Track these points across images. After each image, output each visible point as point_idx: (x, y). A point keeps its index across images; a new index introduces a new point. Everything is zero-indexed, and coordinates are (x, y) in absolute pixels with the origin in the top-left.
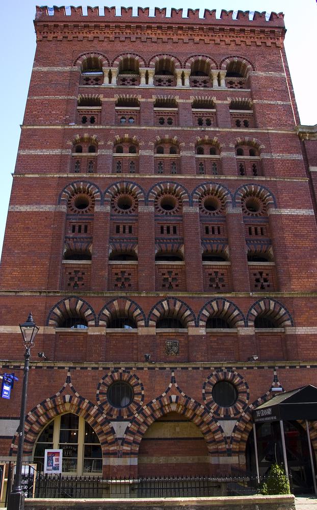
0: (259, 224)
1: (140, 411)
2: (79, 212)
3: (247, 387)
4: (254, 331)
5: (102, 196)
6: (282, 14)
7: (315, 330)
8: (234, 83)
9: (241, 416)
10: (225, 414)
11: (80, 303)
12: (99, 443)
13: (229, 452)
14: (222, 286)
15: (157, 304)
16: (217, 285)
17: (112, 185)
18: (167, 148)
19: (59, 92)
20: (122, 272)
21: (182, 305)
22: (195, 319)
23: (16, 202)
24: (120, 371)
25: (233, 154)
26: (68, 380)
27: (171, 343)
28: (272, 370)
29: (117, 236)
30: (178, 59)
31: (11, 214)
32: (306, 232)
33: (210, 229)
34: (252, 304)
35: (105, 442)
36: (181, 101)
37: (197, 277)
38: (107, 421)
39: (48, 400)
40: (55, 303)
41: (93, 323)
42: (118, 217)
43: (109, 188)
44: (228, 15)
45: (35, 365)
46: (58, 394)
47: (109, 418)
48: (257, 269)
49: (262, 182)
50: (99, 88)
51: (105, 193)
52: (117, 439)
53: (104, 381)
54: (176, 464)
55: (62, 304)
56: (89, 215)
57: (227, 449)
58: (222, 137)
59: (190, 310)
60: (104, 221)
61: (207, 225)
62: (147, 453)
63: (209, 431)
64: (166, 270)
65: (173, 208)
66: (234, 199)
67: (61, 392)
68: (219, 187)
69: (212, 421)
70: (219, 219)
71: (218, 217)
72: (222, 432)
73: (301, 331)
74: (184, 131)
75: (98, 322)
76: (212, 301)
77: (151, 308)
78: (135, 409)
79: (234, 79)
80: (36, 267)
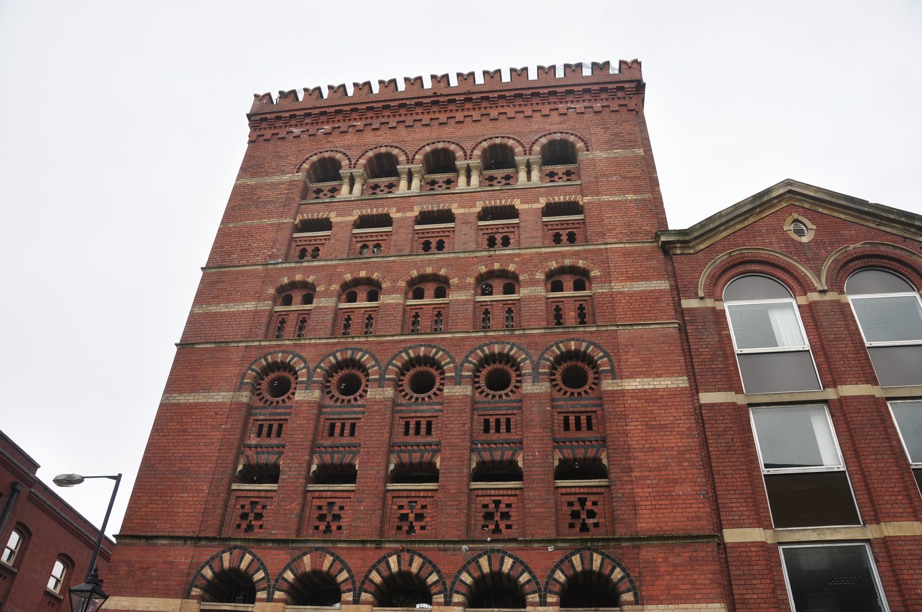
0: (583, 409)
2: (272, 403)
5: (310, 375)
6: (637, 63)
8: (557, 174)
11: (248, 558)
14: (506, 528)
15: (379, 562)
16: (497, 526)
17: (329, 355)
18: (430, 288)
19: (269, 214)
20: (579, 499)
21: (424, 563)
22: (445, 589)
23: (175, 389)
25: (540, 291)
29: (328, 442)
30: (461, 147)
31: (165, 411)
32: (672, 418)
36: (461, 211)
40: (206, 558)
41: (440, 598)
42: (334, 410)
43: (322, 361)
44: (546, 73)
48: (491, 496)
49: (590, 335)
50: (331, 202)
51: (315, 370)
55: (217, 560)
56: (359, 406)
58: (525, 264)
59: (438, 572)
60: (306, 415)
61: (487, 417)
64: (406, 499)
65: (585, 383)
66: (535, 367)
68: (511, 349)
70: (510, 405)
74: (460, 258)
76: (480, 556)
77: (367, 569)
79: (559, 169)
80: (186, 495)
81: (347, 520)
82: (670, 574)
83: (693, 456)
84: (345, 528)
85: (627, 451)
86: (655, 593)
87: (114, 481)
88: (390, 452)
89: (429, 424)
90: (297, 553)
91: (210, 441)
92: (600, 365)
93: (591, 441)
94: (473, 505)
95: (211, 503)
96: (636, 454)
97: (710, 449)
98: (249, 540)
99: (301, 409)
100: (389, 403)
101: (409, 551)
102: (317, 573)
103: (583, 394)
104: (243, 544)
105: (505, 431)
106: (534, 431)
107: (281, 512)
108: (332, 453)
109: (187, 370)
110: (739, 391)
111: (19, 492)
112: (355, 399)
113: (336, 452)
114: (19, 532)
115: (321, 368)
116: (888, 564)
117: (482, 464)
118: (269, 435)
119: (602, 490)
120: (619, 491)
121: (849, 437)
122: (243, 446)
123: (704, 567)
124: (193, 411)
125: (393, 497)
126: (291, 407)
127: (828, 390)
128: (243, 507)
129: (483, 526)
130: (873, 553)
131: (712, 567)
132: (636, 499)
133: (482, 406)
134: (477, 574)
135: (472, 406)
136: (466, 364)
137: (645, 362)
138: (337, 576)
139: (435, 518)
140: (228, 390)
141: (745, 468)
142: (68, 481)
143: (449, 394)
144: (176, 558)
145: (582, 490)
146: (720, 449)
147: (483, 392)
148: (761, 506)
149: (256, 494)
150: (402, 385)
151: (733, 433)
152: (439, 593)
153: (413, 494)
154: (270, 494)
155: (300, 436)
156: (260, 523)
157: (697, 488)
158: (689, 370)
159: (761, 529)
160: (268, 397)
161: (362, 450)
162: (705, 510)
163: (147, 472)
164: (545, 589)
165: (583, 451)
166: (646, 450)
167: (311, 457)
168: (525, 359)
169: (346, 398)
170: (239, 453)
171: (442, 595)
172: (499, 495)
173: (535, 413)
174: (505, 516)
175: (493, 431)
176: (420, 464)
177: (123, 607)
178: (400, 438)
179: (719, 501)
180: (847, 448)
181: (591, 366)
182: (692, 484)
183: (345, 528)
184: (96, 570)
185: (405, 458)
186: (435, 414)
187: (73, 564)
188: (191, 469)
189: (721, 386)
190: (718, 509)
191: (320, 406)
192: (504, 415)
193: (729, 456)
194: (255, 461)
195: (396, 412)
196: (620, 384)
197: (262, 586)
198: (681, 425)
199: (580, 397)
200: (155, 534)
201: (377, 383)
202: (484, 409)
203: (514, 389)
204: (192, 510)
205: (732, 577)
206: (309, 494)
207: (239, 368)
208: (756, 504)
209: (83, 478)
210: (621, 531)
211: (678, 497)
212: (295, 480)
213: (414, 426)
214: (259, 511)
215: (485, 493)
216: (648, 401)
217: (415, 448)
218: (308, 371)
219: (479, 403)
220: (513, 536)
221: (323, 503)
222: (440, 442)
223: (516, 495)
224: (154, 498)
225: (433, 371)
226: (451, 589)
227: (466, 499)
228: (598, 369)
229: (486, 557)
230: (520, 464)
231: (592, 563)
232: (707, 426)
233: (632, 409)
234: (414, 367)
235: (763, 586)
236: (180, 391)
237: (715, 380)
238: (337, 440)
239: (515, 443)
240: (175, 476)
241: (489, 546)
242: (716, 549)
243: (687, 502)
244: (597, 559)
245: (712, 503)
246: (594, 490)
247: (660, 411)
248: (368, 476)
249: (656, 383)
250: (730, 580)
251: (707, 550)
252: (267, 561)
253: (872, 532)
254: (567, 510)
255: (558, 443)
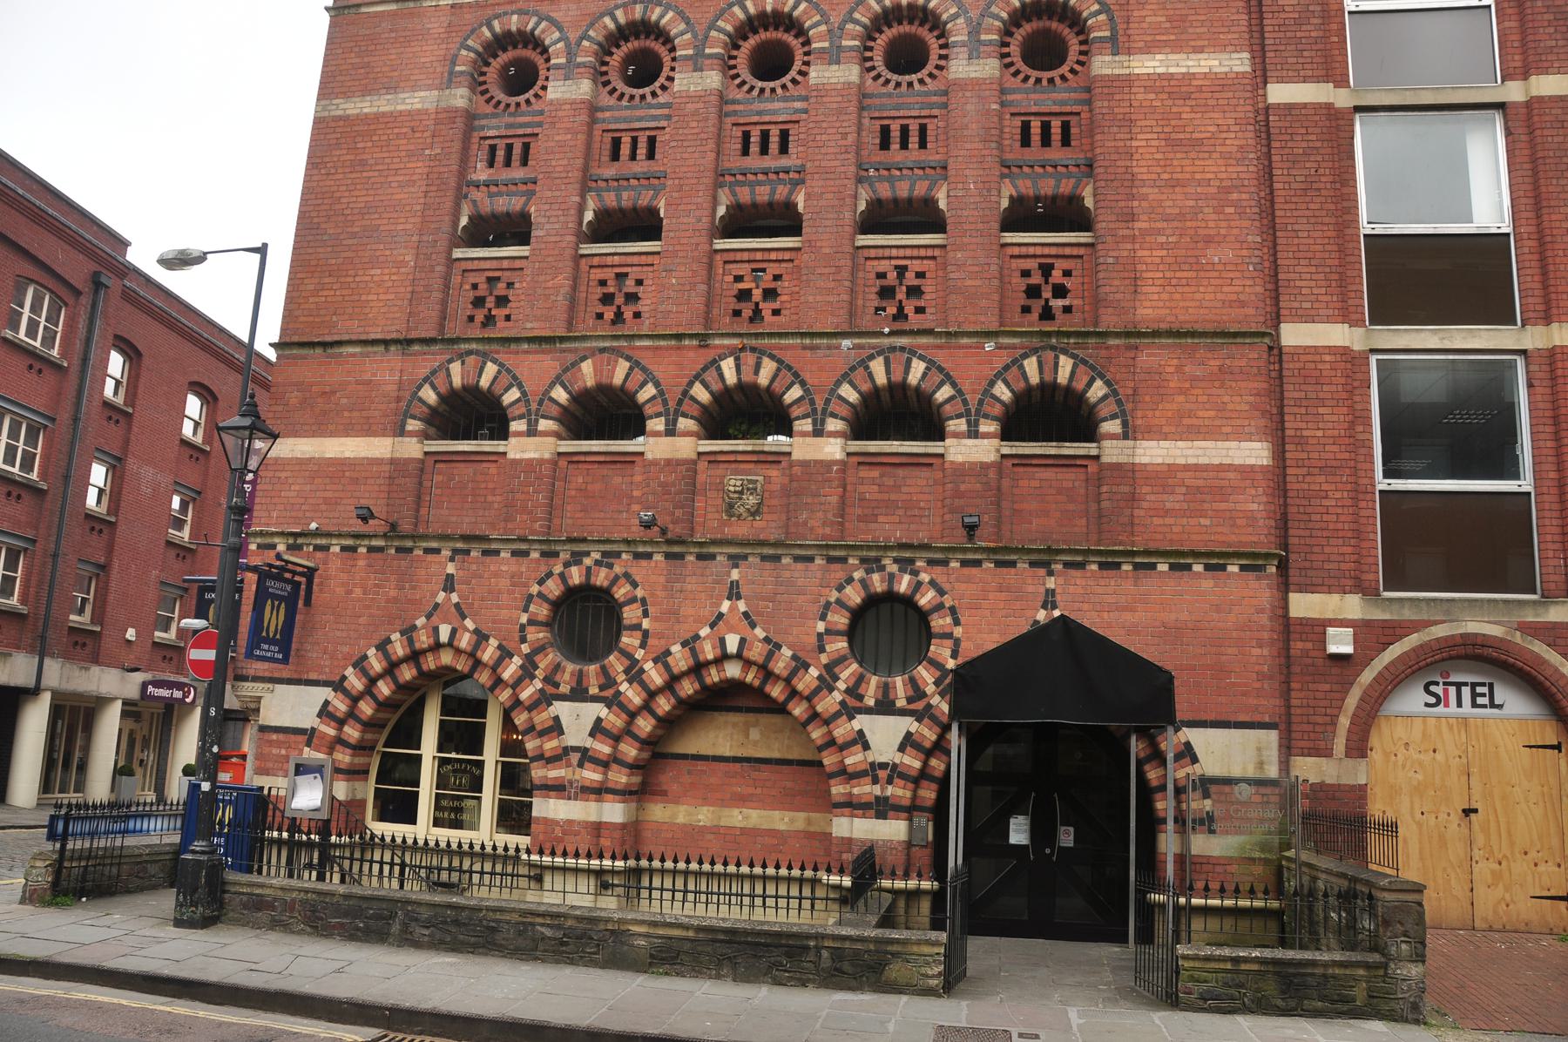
0: (1056, 109)
1: (635, 674)
2: (508, 105)
3: (957, 622)
4: (998, 451)
5: (570, 54)
7: (1200, 452)
9: (929, 706)
10: (880, 697)
11: (491, 369)
12: (526, 756)
13: (882, 808)
15: (705, 369)
16: (901, 308)
17: (602, 15)
20: (1041, 266)
21: (778, 370)
22: (814, 411)
23: (336, 90)
24: (587, 561)
26: (449, 584)
27: (739, 483)
28: (1042, 572)
29: (610, 171)
31: (322, 127)
33: (895, 134)
34: (1000, 366)
35: (540, 757)
37: (832, 285)
38: (544, 699)
39: (395, 636)
40: (425, 372)
42: (616, 114)
43: (592, 25)
45: (366, 542)
46: (421, 622)
47: (550, 690)
48: (890, 258)
52: (567, 750)
53: (542, 589)
54: (744, 831)
56: (661, 106)
57: (877, 798)
59: (803, 384)
61: (886, 122)
62: (664, 793)
63: (831, 742)
64: (746, 265)
66: (975, 31)
67: (428, 617)
69: (837, 715)
70: (926, 99)
71: (927, 94)
72: (866, 747)
73: (1152, 452)
75: (537, 421)
76: (872, 357)
77: (686, 380)
78: (620, 669)
80: (379, 271)
81: (649, 302)
82: (1182, 391)
83: (1244, 196)
84: (647, 315)
85: (1129, 184)
86: (1156, 421)
87: (257, 257)
88: (717, 185)
89: (784, 135)
90: (570, 358)
91: (407, 178)
92: (1092, 29)
93: (1067, 166)
94: (861, 274)
95: (422, 282)
96: (1144, 190)
97: (1276, 186)
98: (490, 340)
99: (560, 114)
100: (712, 98)
101: (753, 349)
102: (604, 389)
103: (1058, 81)
104: (480, 347)
105: (917, 146)
106: (968, 146)
107: (539, 291)
108: (618, 190)
109: (353, 55)
110: (1342, 82)
111: (107, 287)
112: (654, 94)
113: (625, 189)
114: (122, 351)
115: (589, 39)
116: (1548, 391)
117: (876, 204)
118: (508, 163)
119: (1082, 251)
120: (1111, 254)
121: (1530, 173)
122: (464, 185)
123: (1243, 384)
124: (372, 127)
125: (725, 262)
126: (541, 113)
127: (1510, 84)
128: (475, 287)
129: (877, 309)
130: (1527, 372)
131: (1256, 385)
132: (1139, 267)
133: (877, 101)
134: (866, 387)
135: (860, 102)
136: (849, 26)
137: (1175, 24)
138: (637, 392)
139: (796, 296)
140: (429, 88)
141: (1333, 220)
142: (180, 260)
143: (819, 81)
144: (374, 375)
145: (1046, 251)
146: (1294, 186)
147: (879, 76)
148: (1351, 288)
149: (494, 264)
150: (734, 67)
151: (1319, 158)
152: (805, 416)
153: (759, 256)
154: (518, 264)
155: (561, 162)
156: (506, 311)
157: (1245, 252)
158: (1254, 41)
159: (1346, 325)
160: (500, 96)
161: (669, 182)
162: (1254, 290)
163: (310, 238)
164: (978, 413)
165: (1052, 182)
166: (1163, 183)
167: (583, 197)
168: (955, 17)
169: (638, 92)
170: (460, 197)
171: (810, 420)
172: (905, 258)
173: (971, 114)
174: (915, 292)
175: (895, 146)
176: (770, 204)
177: (303, 452)
178: (734, 161)
179: (1280, 276)
180: (1522, 193)
181: (1075, 30)
182: (1238, 245)
183: (647, 315)
184: (252, 396)
185: (745, 195)
186: (794, 118)
187: (215, 399)
188: (382, 228)
189: (1310, 73)
190: (1276, 290)
191: (593, 109)
192: (915, 117)
193: (1307, 199)
194: (488, 209)
195: (727, 115)
196: (1126, 64)
197: (517, 413)
198: (1228, 142)
199: (1051, 87)
200: (336, 338)
201: (690, 63)
202: (881, 108)
203: (935, 72)
204: (392, 297)
205: (1286, 402)
206: (583, 261)
207: (444, 46)
208: (1343, 284)
209: (205, 254)
210: (1109, 321)
211: (1209, 267)
212: (558, 238)
213: (758, 139)
214: (503, 293)
215: (881, 253)
216: (1174, 96)
217: (761, 177)
218: (568, 45)
219: (871, 96)
220: (927, 326)
221: (609, 274)
222: (803, 165)
223: (934, 258)
224: (326, 280)
225: (789, 38)
226: (824, 411)
227: (849, 263)
228: (1088, 35)
229: (881, 359)
230: (942, 205)
231: (1056, 372)
232: (1274, 144)
233: (1143, 110)
234: (755, 32)
235: (1335, 418)
236: (347, 95)
237: (1301, 60)
238: (625, 166)
239: (934, 168)
240: (355, 241)
241: (886, 341)
242: (1265, 356)
243: (1224, 275)
244: (1066, 365)
245: (1268, 279)
246: (1068, 251)
247: (1193, 115)
248: (682, 227)
249: (1190, 63)
250: (1282, 407)
251: (1251, 356)
252: (523, 373)
253: (1534, 338)
254: (1021, 284)
255: (1008, 168)
